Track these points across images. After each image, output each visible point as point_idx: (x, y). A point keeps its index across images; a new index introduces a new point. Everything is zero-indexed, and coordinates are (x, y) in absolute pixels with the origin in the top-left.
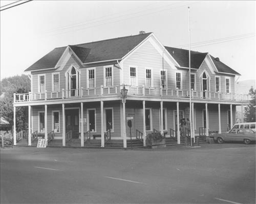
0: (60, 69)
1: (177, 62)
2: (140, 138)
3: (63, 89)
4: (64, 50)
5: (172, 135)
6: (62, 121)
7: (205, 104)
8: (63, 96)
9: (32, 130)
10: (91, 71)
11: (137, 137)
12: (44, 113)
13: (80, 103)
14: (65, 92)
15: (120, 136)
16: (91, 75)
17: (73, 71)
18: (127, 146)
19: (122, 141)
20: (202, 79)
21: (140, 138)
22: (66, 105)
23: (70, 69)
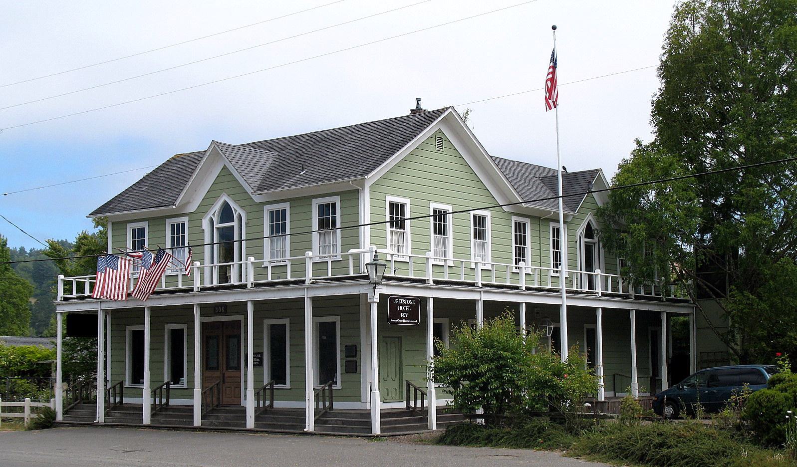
0: (192, 208)
1: (398, 277)
2: (419, 404)
3: (198, 264)
4: (202, 157)
5: (412, 404)
6: (191, 381)
7: (595, 309)
8: (197, 284)
9: (109, 378)
10: (278, 212)
11: (408, 403)
12: (142, 333)
13: (245, 304)
14: (202, 273)
15: (358, 398)
16: (278, 225)
17: (226, 213)
18: (256, 425)
19: (368, 415)
20: (584, 240)
21: (419, 404)
22: (206, 309)
23: (217, 207)
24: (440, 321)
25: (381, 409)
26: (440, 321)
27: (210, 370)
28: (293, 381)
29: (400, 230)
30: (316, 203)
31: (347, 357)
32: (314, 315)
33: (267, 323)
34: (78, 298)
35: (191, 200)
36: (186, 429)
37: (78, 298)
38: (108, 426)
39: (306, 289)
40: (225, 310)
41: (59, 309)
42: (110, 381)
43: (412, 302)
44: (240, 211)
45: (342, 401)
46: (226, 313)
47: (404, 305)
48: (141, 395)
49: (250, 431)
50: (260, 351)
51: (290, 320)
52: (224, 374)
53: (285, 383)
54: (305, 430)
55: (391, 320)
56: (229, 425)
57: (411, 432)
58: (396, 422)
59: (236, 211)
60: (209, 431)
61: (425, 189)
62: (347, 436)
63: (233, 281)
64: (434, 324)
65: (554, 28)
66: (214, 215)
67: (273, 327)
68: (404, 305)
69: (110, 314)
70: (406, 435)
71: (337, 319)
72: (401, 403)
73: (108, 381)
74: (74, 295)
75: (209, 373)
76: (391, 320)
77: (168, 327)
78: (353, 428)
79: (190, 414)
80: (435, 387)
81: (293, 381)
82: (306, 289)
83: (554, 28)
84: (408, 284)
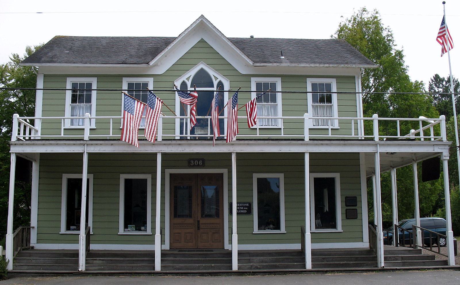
6: (153, 228)
18: (313, 266)
27: (179, 217)
30: (309, 82)
31: (346, 206)
32: (310, 172)
34: (366, 139)
35: (159, 64)
36: (149, 274)
37: (366, 139)
38: (166, 274)
39: (86, 145)
40: (189, 162)
41: (13, 150)
42: (36, 227)
44: (220, 78)
46: (204, 166)
48: (77, 241)
49: (310, 271)
50: (247, 200)
52: (198, 222)
54: (80, 270)
56: (276, 267)
59: (216, 78)
60: (91, 275)
62: (432, 269)
65: (444, 3)
66: (188, 79)
67: (69, 180)
69: (38, 161)
71: (337, 176)
73: (33, 227)
74: (189, 136)
75: (178, 220)
77: (256, 176)
78: (424, 262)
79: (151, 259)
82: (86, 145)
83: (444, 3)
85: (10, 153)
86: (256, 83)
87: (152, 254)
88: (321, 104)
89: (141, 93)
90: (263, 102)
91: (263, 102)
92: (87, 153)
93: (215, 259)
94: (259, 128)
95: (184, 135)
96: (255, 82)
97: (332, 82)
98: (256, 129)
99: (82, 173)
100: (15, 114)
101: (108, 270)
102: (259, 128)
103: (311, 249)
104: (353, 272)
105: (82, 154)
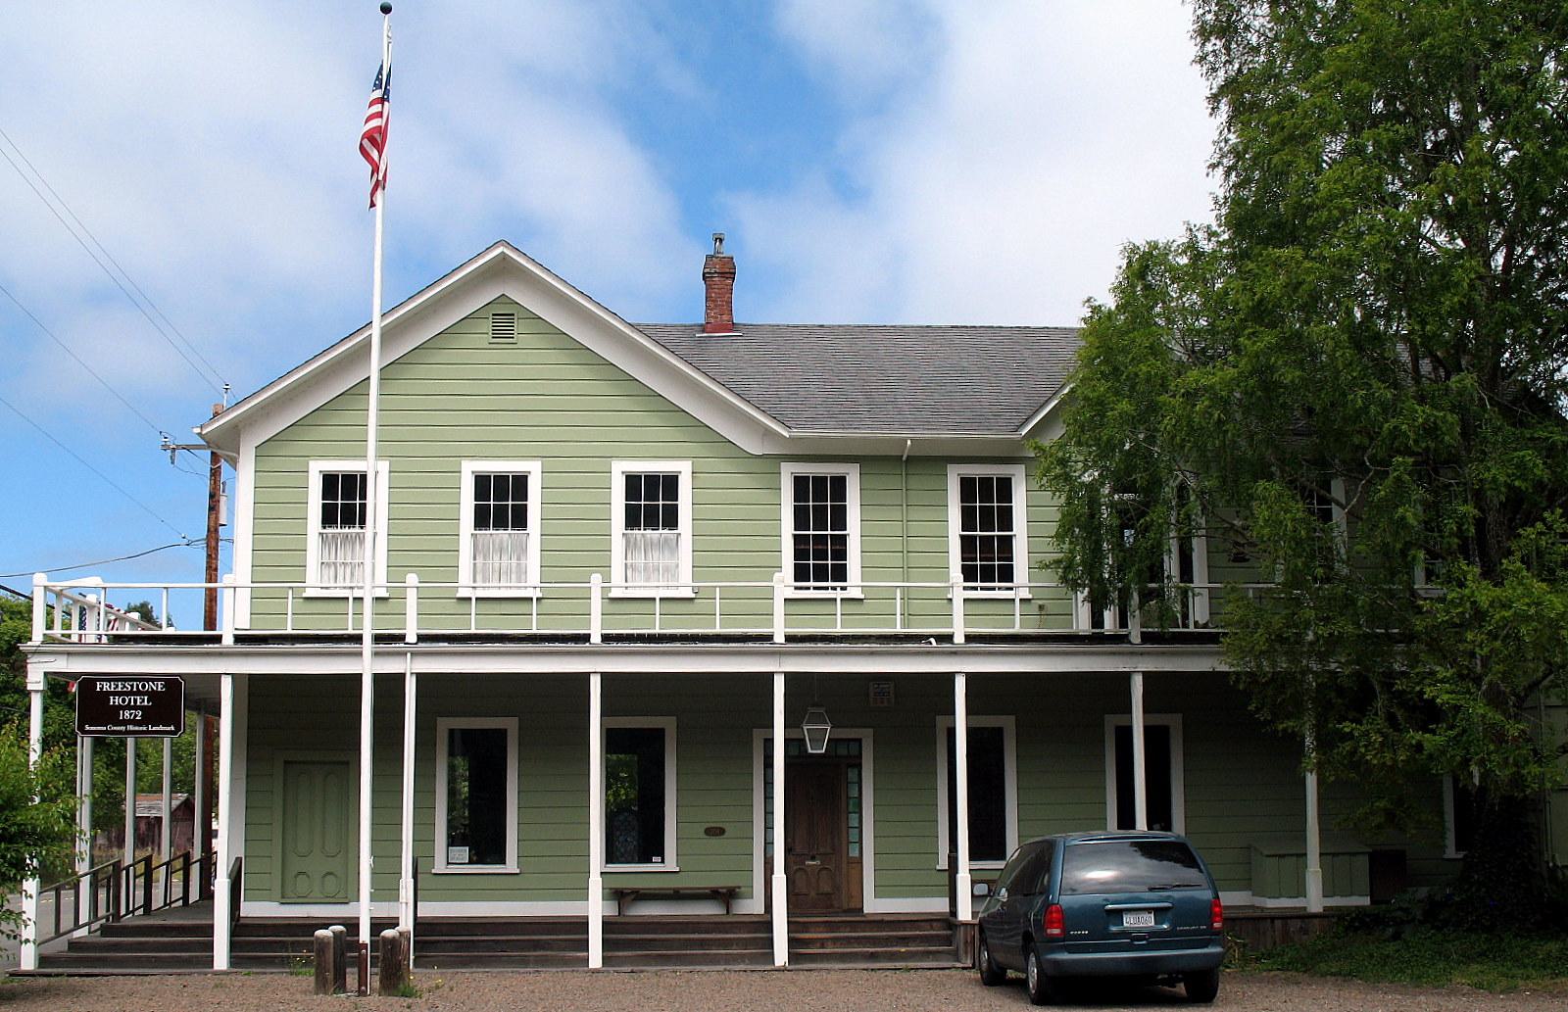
24: (1159, 720)
25: (371, 918)
26: (1159, 720)
28: (249, 856)
29: (339, 530)
33: (444, 724)
39: (409, 655)
43: (160, 687)
45: (385, 901)
47: (138, 693)
51: (678, 719)
53: (503, 861)
55: (87, 728)
57: (110, 971)
58: (141, 947)
61: (953, 428)
63: (83, 642)
64: (1147, 730)
68: (138, 693)
70: (811, 970)
72: (343, 906)
76: (87, 728)
80: (602, 873)
81: (249, 856)
82: (409, 655)
84: (677, 646)
85: (30, 692)
86: (795, 477)
87: (582, 925)
88: (346, 530)
89: (829, 503)
90: (642, 528)
91: (642, 528)
92: (412, 674)
93: (475, 938)
94: (1021, 600)
95: (57, 631)
96: (959, 475)
97: (848, 474)
98: (835, 599)
99: (1129, 711)
100: (225, 576)
101: (696, 954)
102: (1021, 600)
103: (587, 900)
104: (297, 974)
105: (769, 677)
